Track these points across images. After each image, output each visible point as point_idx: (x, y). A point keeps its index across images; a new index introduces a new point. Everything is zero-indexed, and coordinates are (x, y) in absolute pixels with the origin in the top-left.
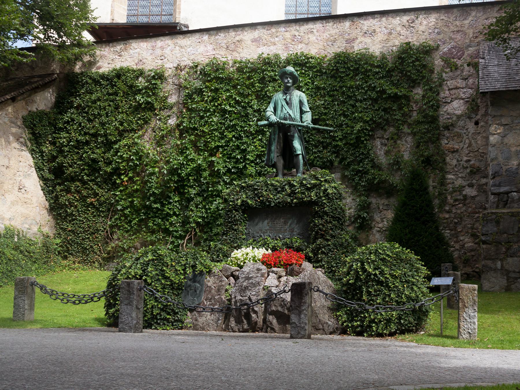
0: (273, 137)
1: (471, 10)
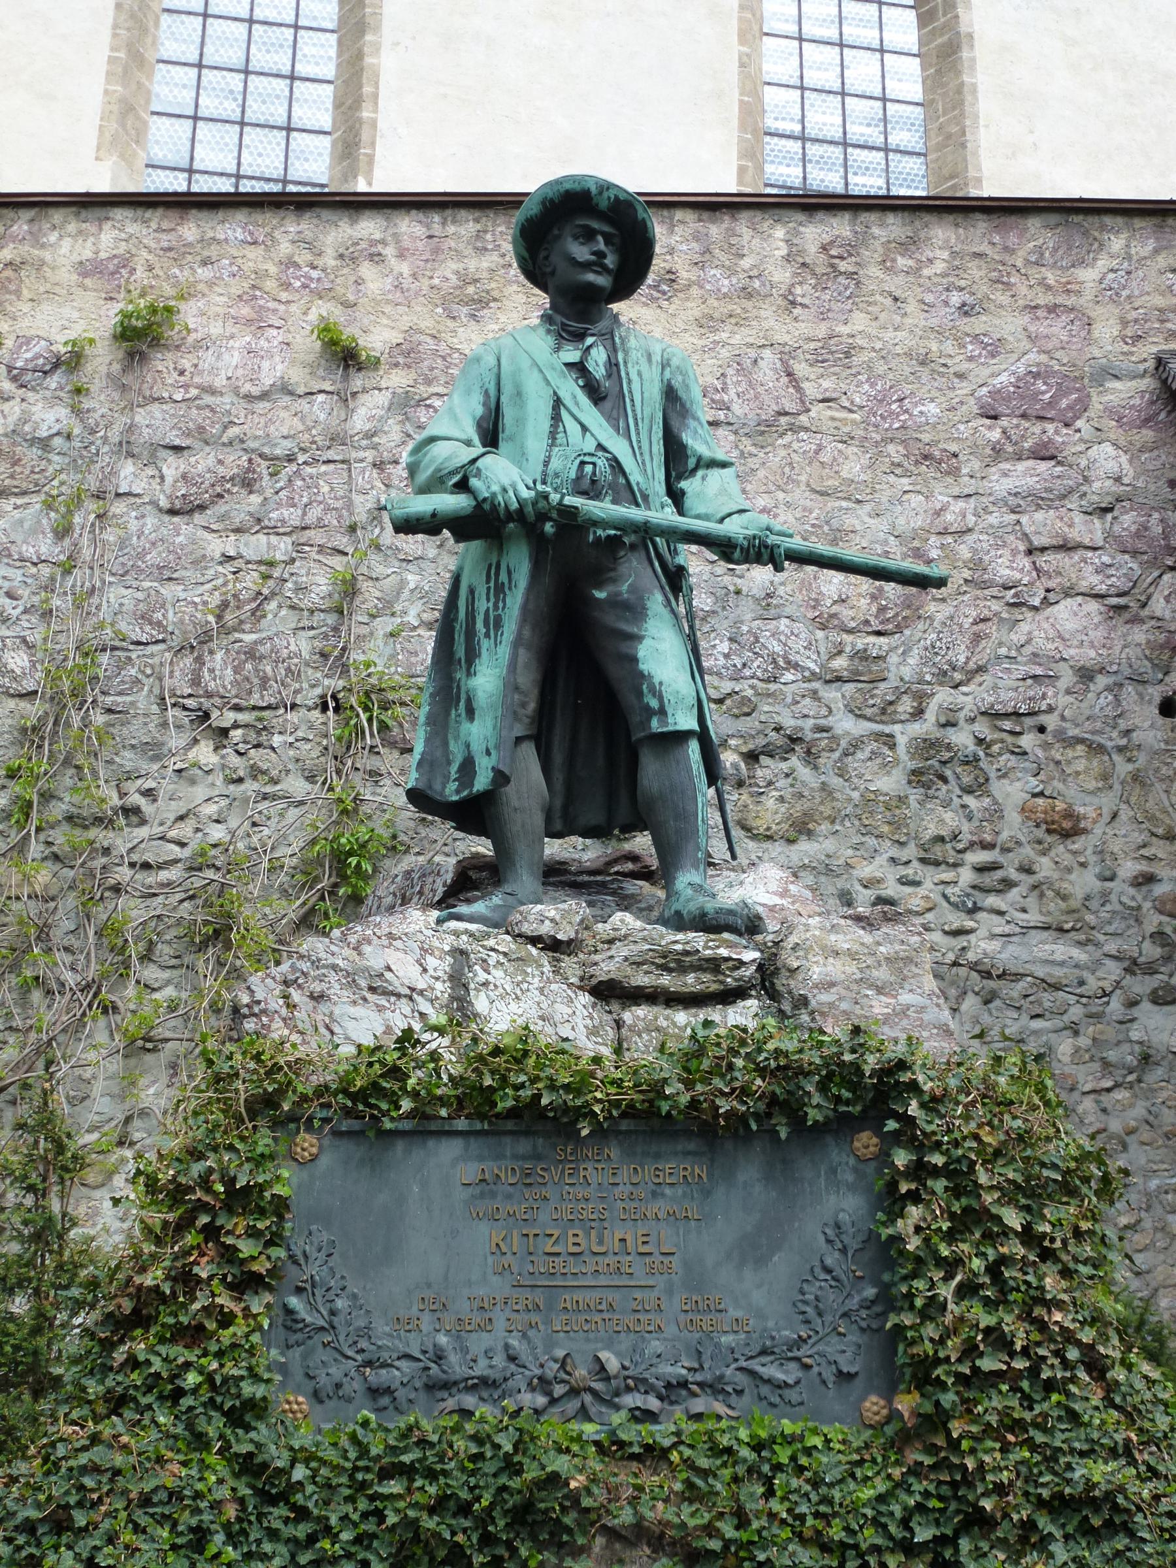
1: (1103, 228)
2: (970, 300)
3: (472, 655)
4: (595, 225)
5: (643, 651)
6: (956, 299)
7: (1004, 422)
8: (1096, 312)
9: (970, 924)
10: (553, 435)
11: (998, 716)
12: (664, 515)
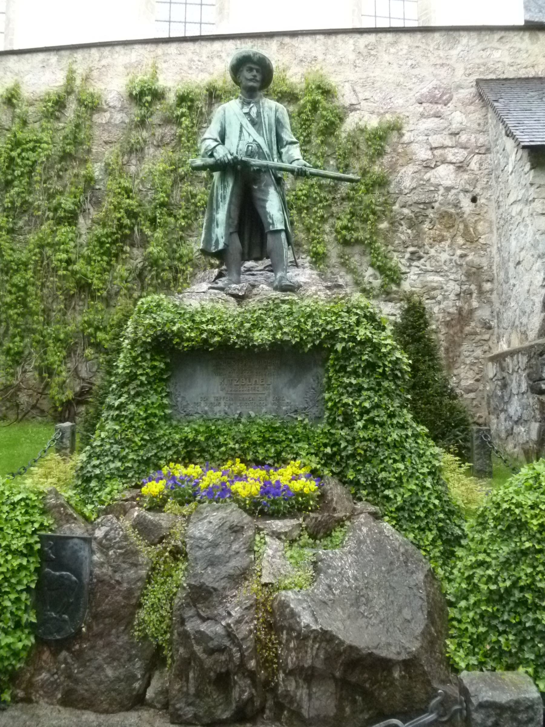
0: (220, 192)
1: (460, 36)
2: (414, 63)
3: (218, 207)
4: (253, 66)
5: (268, 205)
6: (410, 62)
7: (424, 105)
8: (456, 66)
9: (408, 271)
10: (240, 137)
11: (420, 204)
12: (276, 163)
